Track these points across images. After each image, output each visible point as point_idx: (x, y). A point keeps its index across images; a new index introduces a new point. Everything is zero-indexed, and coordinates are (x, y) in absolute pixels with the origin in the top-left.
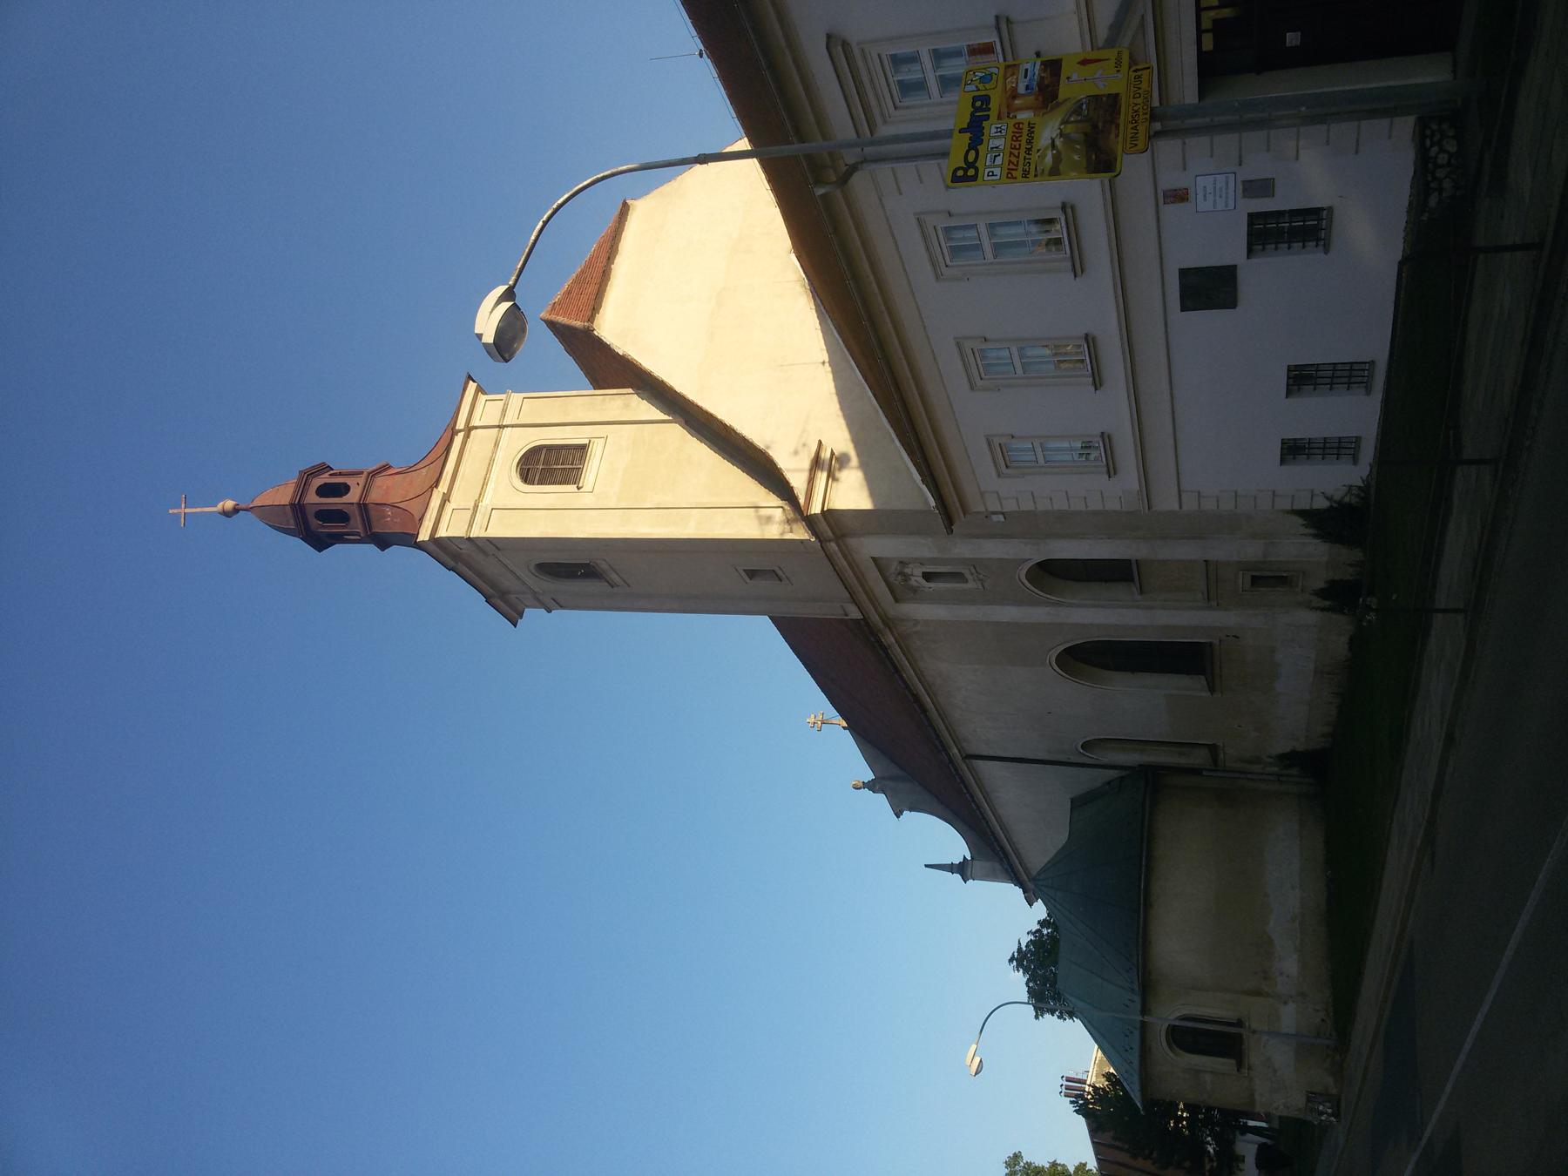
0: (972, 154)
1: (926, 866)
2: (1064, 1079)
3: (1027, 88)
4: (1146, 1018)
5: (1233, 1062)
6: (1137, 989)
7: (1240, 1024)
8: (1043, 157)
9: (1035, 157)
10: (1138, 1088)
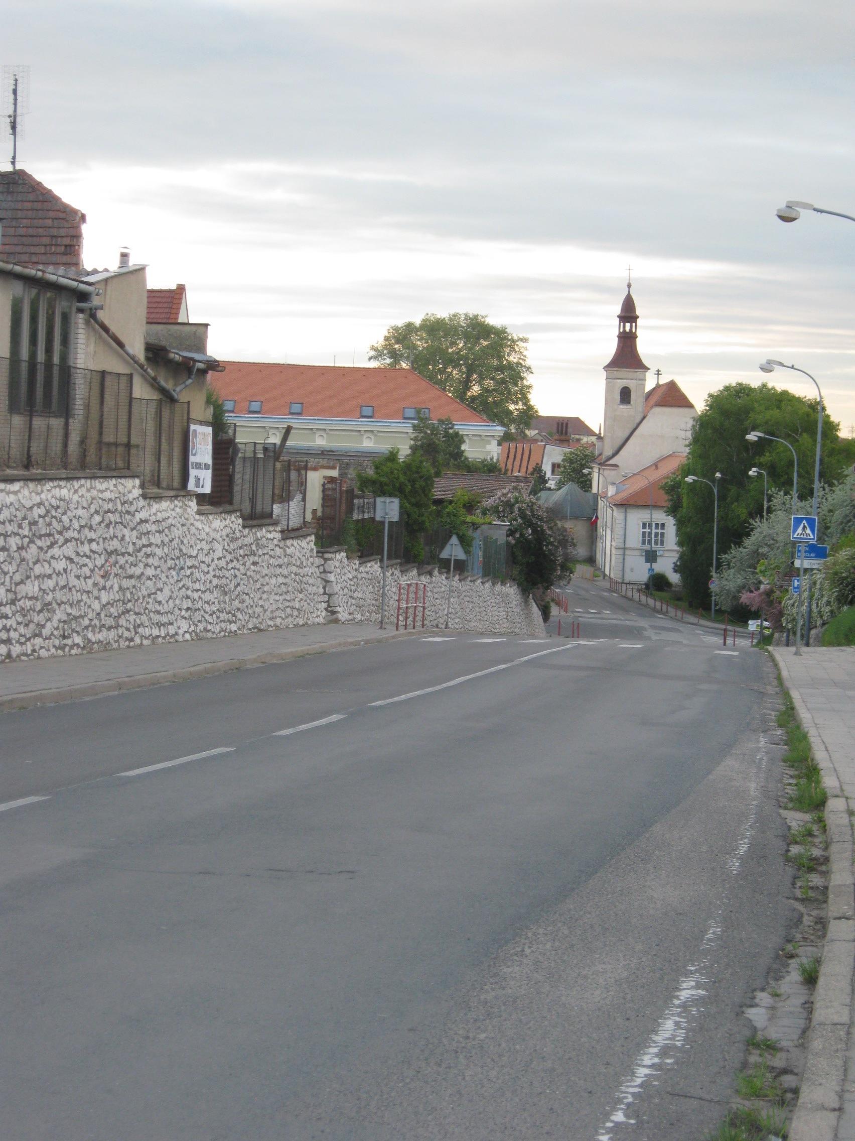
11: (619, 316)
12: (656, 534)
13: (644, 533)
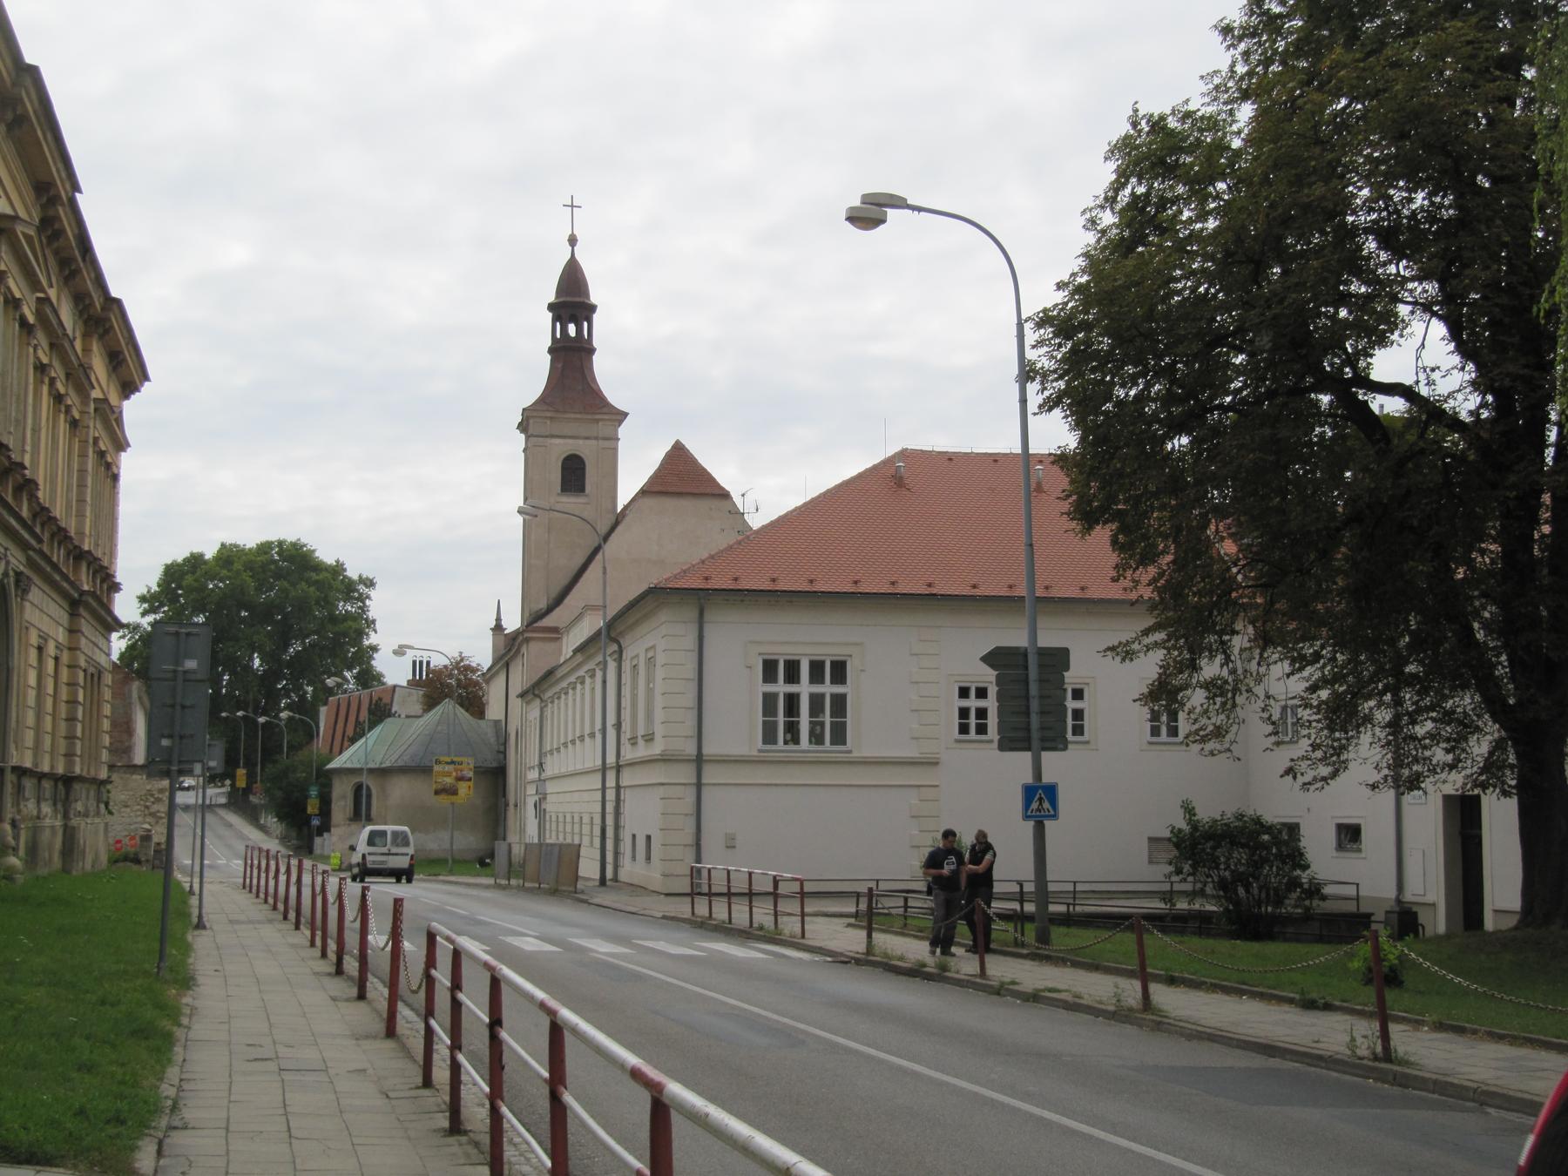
11: (551, 307)
12: (816, 702)
13: (769, 701)
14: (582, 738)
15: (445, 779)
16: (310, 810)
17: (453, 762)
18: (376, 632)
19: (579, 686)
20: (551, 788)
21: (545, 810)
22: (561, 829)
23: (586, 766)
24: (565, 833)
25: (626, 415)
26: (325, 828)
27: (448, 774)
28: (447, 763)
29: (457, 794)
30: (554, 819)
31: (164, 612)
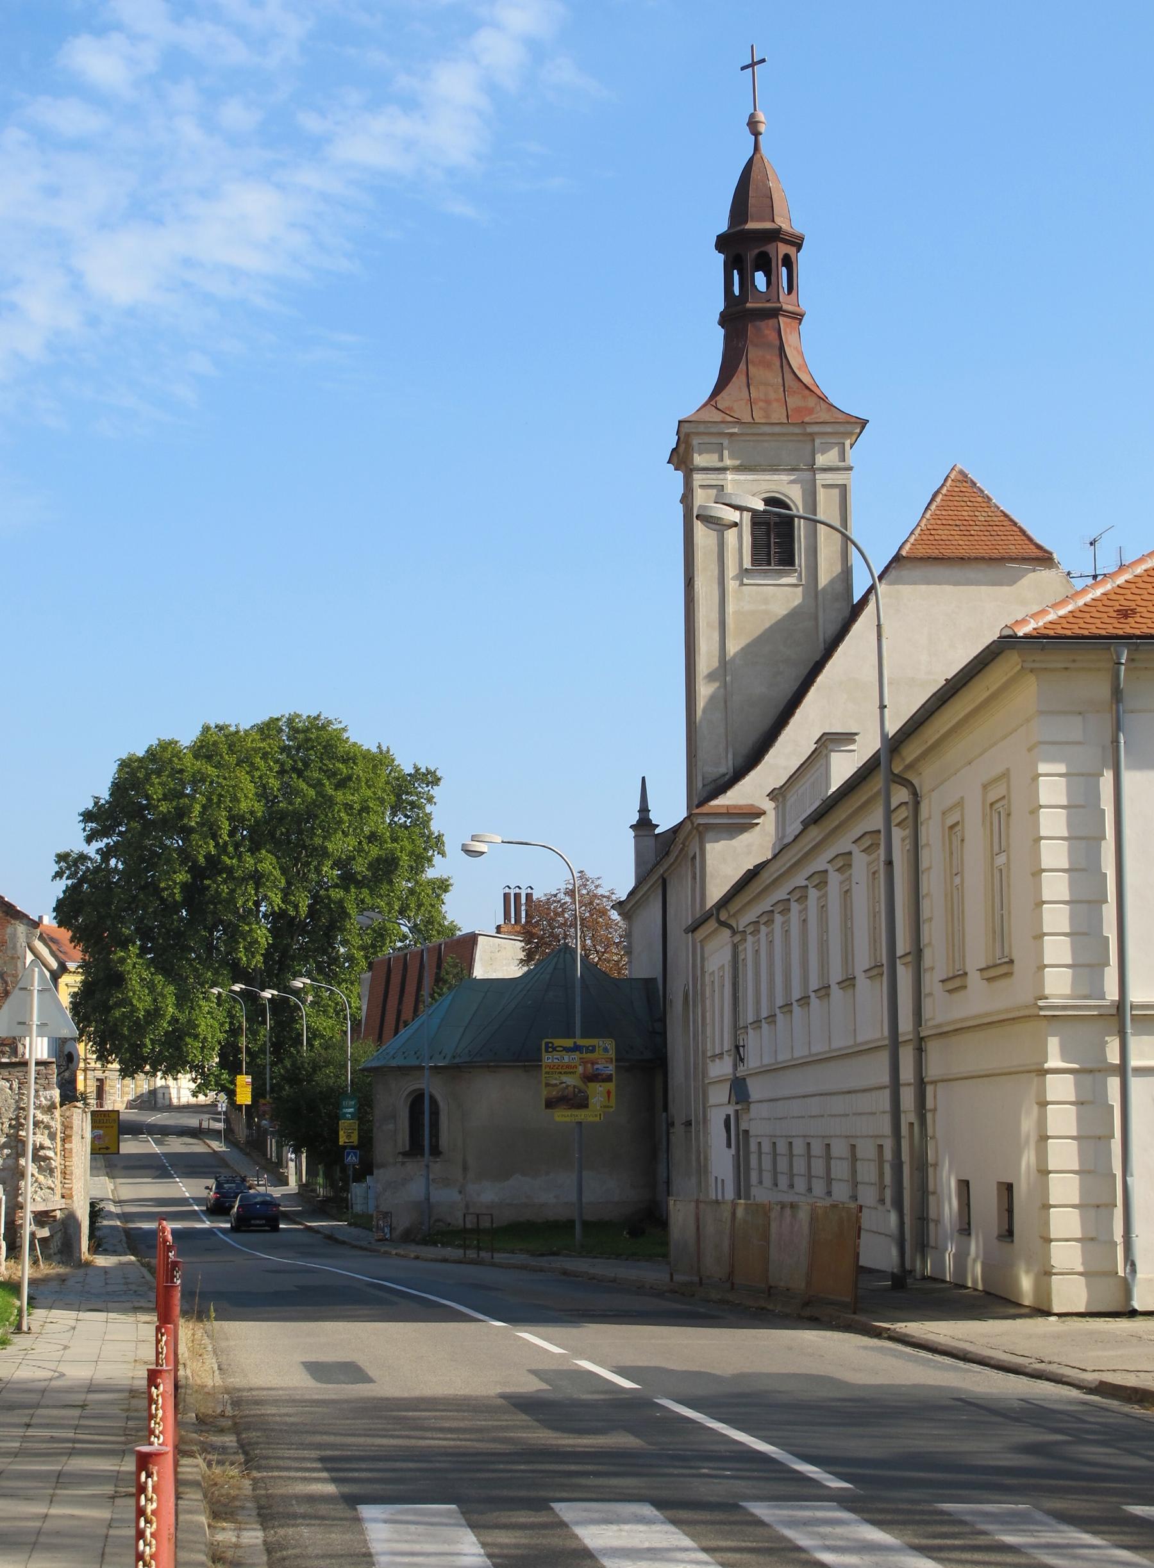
0: (561, 1049)
1: (643, 778)
2: (529, 891)
3: (597, 1069)
4: (427, 1072)
5: (407, 1148)
6: (454, 1062)
7: (436, 1151)
8: (556, 1079)
9: (557, 1076)
10: (374, 1065)
14: (824, 991)
15: (564, 1078)
16: (342, 1140)
17: (577, 1048)
18: (443, 854)
19: (795, 907)
20: (756, 1090)
21: (746, 1132)
22: (782, 1164)
23: (814, 1050)
24: (810, 1177)
25: (864, 423)
26: (366, 1169)
27: (569, 1070)
28: (567, 1050)
29: (586, 1106)
30: (766, 1147)
31: (120, 834)
